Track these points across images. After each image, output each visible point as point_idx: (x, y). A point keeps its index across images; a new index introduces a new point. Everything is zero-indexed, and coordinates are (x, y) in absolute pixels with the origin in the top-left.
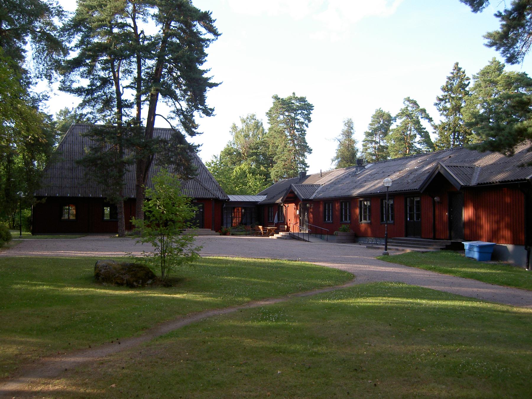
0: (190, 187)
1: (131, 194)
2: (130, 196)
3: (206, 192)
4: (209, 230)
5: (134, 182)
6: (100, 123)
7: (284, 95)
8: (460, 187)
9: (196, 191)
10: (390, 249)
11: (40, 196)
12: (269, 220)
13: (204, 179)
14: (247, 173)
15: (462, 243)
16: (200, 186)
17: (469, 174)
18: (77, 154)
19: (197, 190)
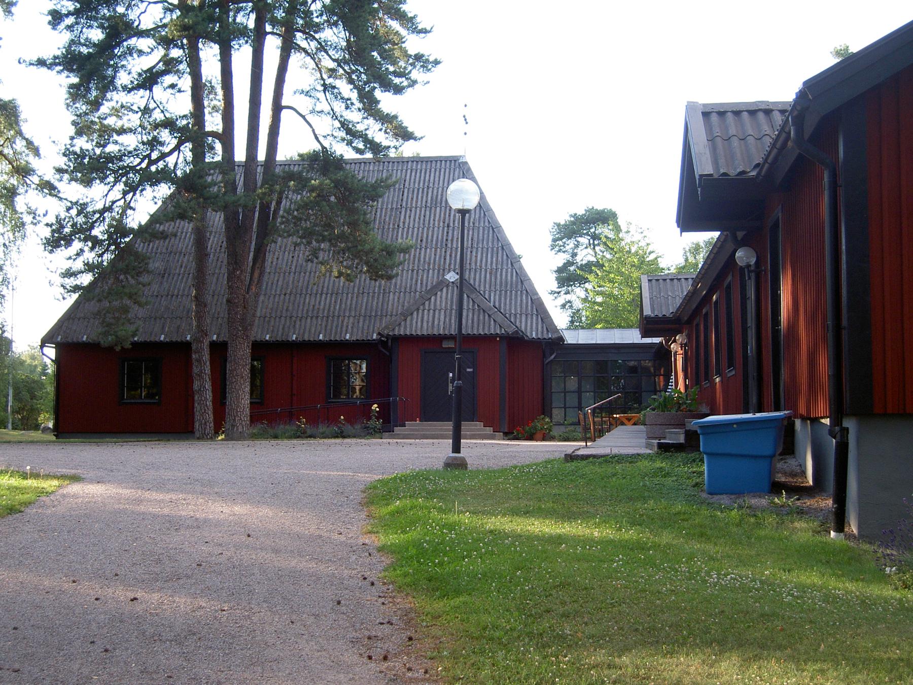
0: (438, 307)
2: (287, 335)
3: (481, 317)
5: (307, 300)
11: (70, 341)
13: (501, 286)
14: (318, 245)
18: (186, 236)
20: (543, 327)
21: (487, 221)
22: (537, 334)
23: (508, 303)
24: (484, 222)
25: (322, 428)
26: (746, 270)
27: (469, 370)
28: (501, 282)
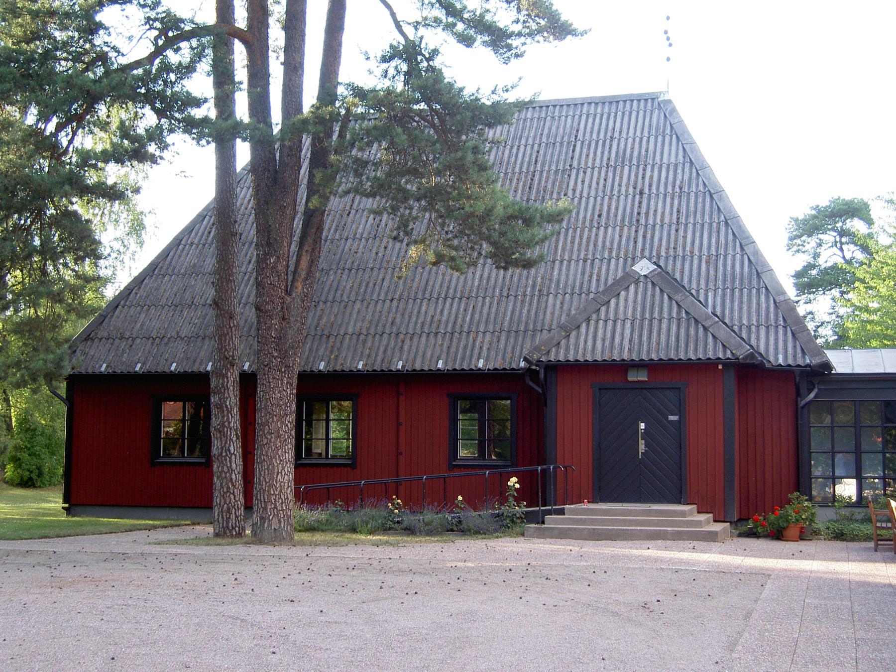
0: (621, 316)
1: (397, 354)
6: (88, 117)
9: (645, 332)
19: (651, 325)
27: (671, 418)
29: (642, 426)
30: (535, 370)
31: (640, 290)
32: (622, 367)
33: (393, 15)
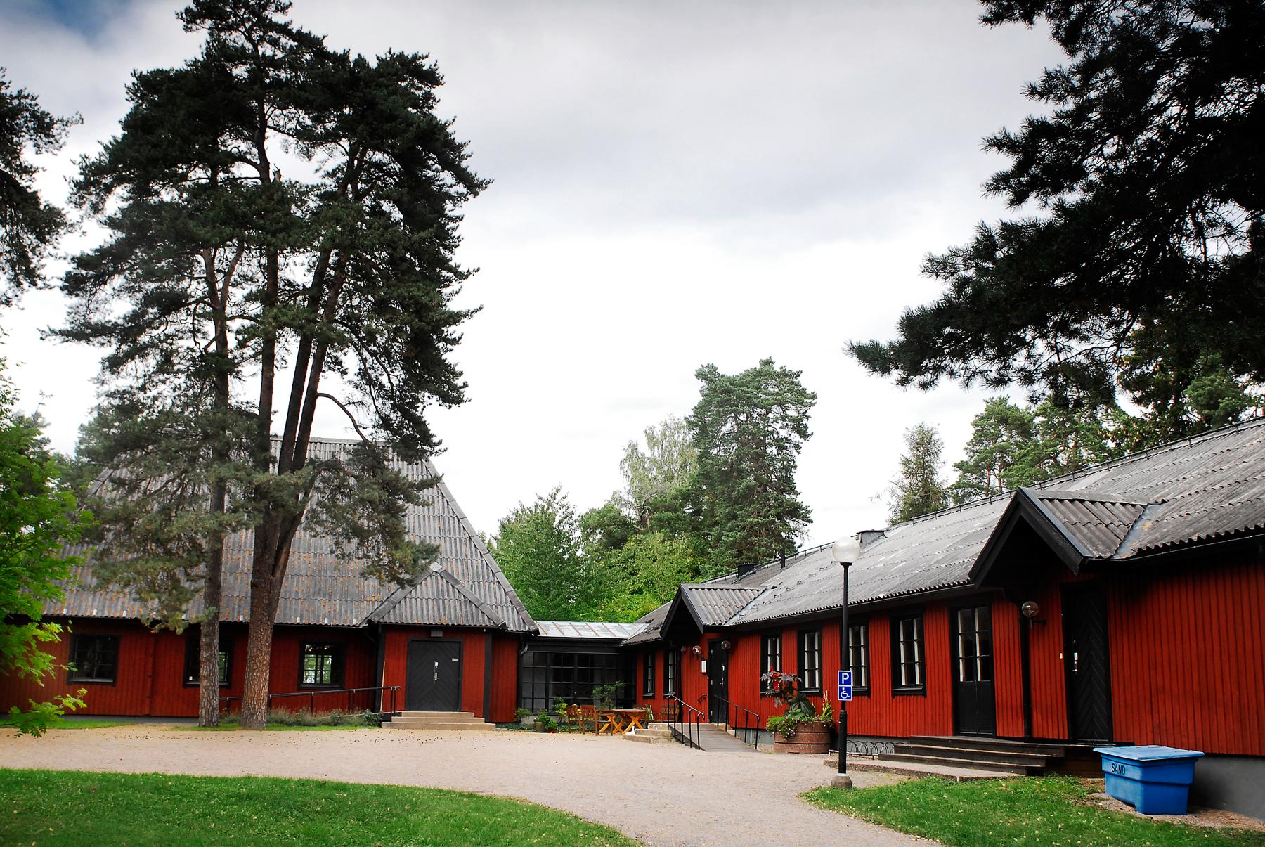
4: (468, 716)
7: (733, 366)
8: (1079, 561)
10: (853, 767)
12: (646, 691)
15: (1095, 750)
16: (454, 592)
17: (1117, 523)
20: (519, 619)
21: (451, 511)
22: (515, 626)
23: (483, 594)
24: (449, 512)
25: (355, 716)
26: (1031, 621)
27: (453, 660)
28: (473, 573)
29: (436, 664)
30: (161, 630)
31: (434, 580)
32: (428, 629)
33: (353, 421)
